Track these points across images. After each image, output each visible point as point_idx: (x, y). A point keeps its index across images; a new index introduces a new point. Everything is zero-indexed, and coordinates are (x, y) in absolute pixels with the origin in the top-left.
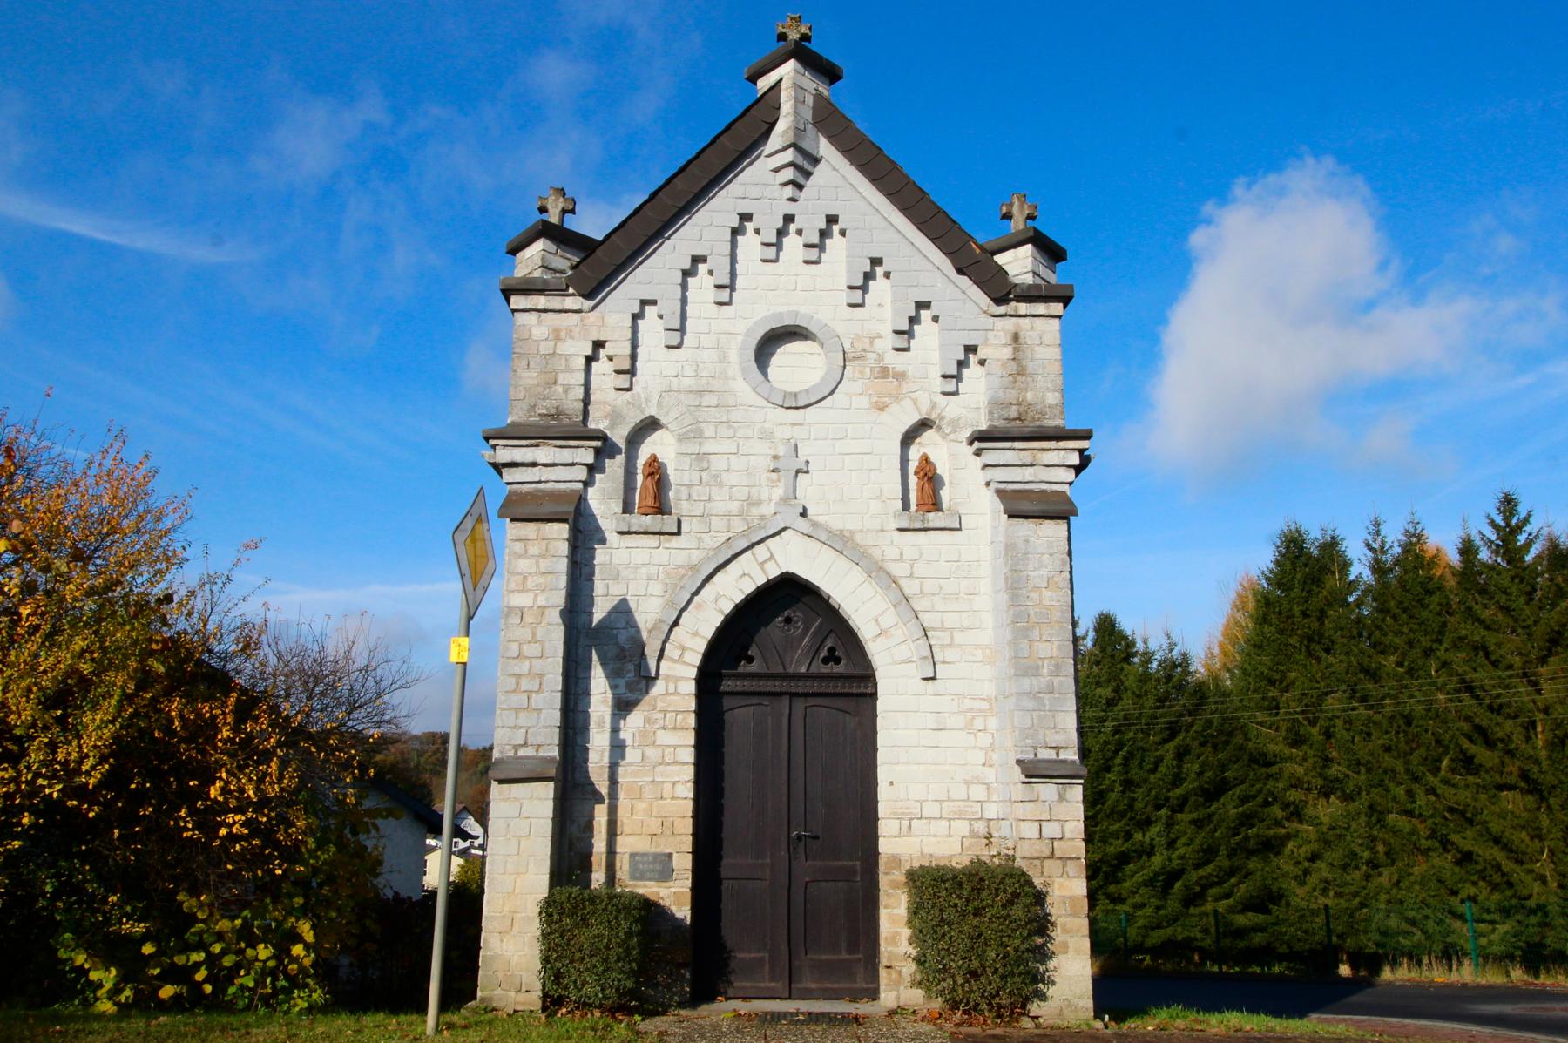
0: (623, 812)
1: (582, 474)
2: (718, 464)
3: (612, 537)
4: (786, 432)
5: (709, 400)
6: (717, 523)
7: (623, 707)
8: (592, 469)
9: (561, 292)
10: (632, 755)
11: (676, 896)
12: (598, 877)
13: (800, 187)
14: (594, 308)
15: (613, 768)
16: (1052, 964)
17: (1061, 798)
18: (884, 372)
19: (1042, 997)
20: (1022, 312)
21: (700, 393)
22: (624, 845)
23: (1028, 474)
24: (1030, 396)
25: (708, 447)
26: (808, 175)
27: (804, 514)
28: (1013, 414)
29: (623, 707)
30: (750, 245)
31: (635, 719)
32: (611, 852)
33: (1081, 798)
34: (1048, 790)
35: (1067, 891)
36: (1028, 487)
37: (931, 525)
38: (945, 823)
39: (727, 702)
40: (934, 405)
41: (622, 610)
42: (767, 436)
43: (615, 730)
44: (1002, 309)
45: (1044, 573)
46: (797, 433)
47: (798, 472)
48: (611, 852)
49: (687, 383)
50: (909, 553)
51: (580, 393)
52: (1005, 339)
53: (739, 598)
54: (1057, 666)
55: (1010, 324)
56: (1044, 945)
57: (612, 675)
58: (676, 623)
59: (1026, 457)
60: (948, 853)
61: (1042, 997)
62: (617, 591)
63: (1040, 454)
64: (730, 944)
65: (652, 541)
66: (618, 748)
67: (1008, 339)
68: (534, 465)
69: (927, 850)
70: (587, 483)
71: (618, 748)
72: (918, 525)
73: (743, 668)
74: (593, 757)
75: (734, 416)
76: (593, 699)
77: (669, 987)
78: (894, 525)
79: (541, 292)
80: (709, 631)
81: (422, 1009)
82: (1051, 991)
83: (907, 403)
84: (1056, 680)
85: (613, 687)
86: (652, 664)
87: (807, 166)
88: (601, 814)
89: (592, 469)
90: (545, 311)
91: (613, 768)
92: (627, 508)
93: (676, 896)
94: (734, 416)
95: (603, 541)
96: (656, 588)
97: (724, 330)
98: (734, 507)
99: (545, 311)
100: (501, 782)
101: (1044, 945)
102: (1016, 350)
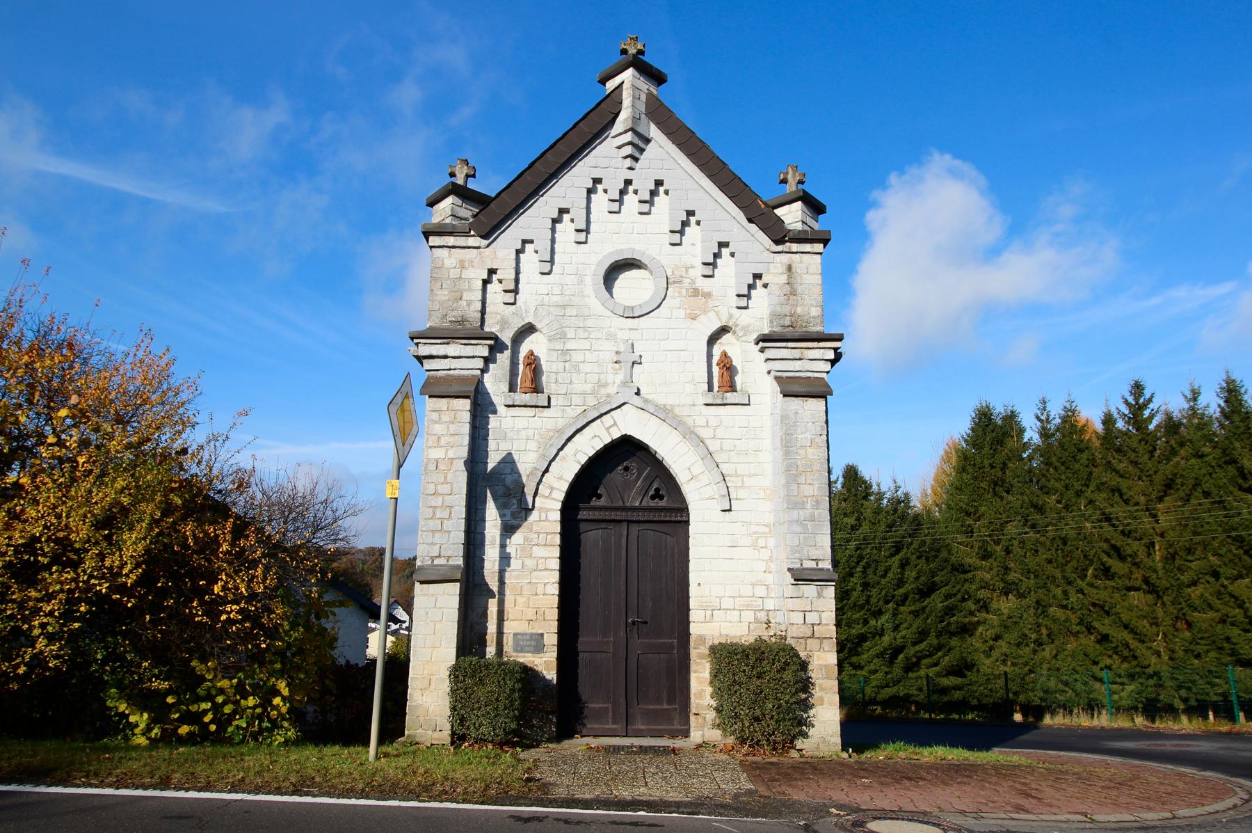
1: (480, 364)
2: (577, 357)
3: (501, 409)
5: (570, 311)
6: (576, 400)
7: (508, 529)
8: (488, 360)
10: (515, 564)
11: (546, 664)
12: (491, 650)
13: (636, 160)
14: (489, 245)
16: (812, 713)
17: (820, 595)
18: (696, 292)
19: (805, 735)
21: (564, 306)
22: (509, 628)
23: (797, 365)
24: (799, 310)
26: (642, 151)
27: (638, 393)
29: (508, 529)
30: (599, 200)
31: (517, 539)
32: (500, 632)
34: (810, 590)
35: (823, 661)
39: (583, 526)
40: (731, 316)
41: (508, 461)
43: (503, 546)
44: (780, 248)
45: (809, 436)
46: (633, 336)
48: (500, 632)
51: (479, 306)
56: (807, 698)
57: (501, 507)
59: (797, 354)
60: (739, 634)
61: (805, 735)
66: (505, 559)
69: (723, 632)
70: (484, 370)
71: (505, 559)
73: (595, 502)
75: (589, 323)
77: (541, 728)
79: (451, 234)
81: (366, 743)
82: (811, 732)
83: (712, 314)
84: (816, 512)
87: (641, 145)
88: (493, 605)
89: (488, 360)
90: (454, 247)
92: (512, 388)
93: (546, 664)
94: (589, 323)
95: (495, 412)
96: (532, 445)
98: (588, 388)
99: (454, 247)
101: (807, 698)
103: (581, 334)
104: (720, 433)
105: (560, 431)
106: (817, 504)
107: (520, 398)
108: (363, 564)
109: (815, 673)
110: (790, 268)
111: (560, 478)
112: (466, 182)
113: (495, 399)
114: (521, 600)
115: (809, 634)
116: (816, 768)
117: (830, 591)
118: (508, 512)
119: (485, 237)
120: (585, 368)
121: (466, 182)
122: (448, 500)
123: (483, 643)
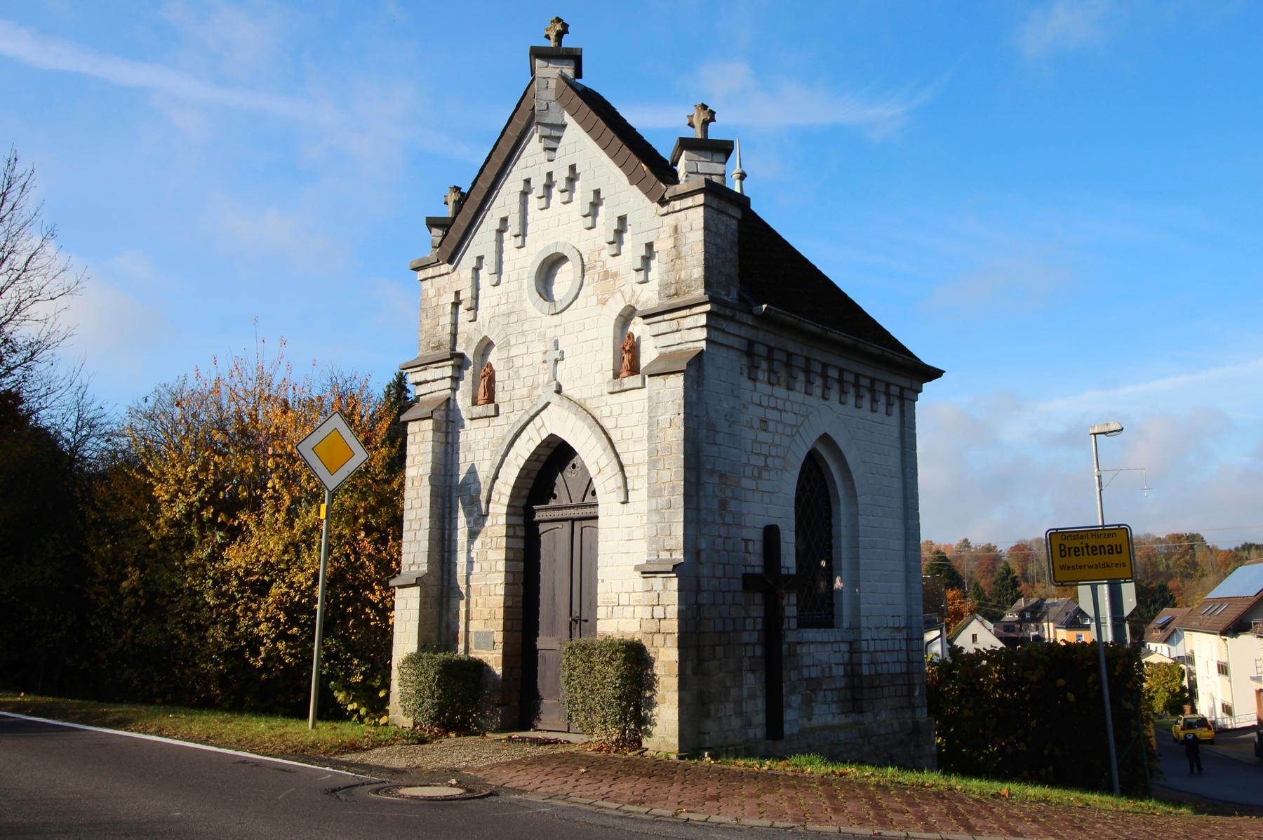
0: (472, 605)
1: (448, 383)
2: (518, 362)
3: (467, 422)
4: (551, 333)
5: (514, 318)
6: (518, 405)
7: (473, 535)
8: (456, 379)
9: (437, 263)
10: (476, 567)
11: (493, 658)
12: (461, 647)
13: (554, 150)
14: (454, 269)
15: (468, 575)
16: (655, 711)
17: (665, 587)
18: (606, 275)
19: (649, 734)
20: (677, 208)
21: (508, 315)
22: (474, 626)
23: (677, 338)
24: (683, 275)
25: (513, 352)
26: (559, 139)
27: (559, 391)
28: (673, 291)
29: (473, 535)
30: (534, 201)
31: (478, 543)
32: (467, 631)
33: (676, 587)
34: (657, 582)
35: (666, 658)
36: (679, 347)
37: (626, 387)
38: (631, 609)
39: (542, 528)
40: (633, 293)
41: (472, 472)
42: (542, 337)
43: (469, 551)
44: (665, 209)
45: (668, 416)
46: (557, 333)
47: (556, 361)
48: (467, 631)
49: (503, 308)
50: (616, 411)
51: (448, 329)
52: (669, 231)
53: (527, 456)
54: (673, 488)
55: (671, 219)
56: (651, 697)
57: (468, 514)
58: (496, 477)
59: (674, 324)
60: (633, 630)
61: (649, 734)
62: (470, 458)
63: (682, 321)
64: (541, 693)
65: (485, 422)
66: (470, 562)
67: (671, 232)
68: (427, 382)
69: (621, 629)
70: (454, 389)
71: (470, 562)
72: (618, 389)
73: (553, 503)
74: (459, 569)
75: (526, 327)
76: (459, 532)
77: (491, 719)
78: (605, 392)
79: (428, 266)
80: (512, 481)
81: (304, 716)
82: (655, 730)
83: (618, 295)
84: (672, 498)
85: (468, 523)
86: (483, 505)
87: (555, 133)
88: (462, 604)
89: (456, 379)
90: (433, 277)
91: (468, 575)
92: (474, 403)
93: (493, 658)
94: (526, 327)
95: (463, 427)
96: (487, 454)
97: (522, 262)
98: (525, 391)
99: (433, 277)
100: (400, 587)
101: (651, 697)
102: (676, 239)
103: (521, 340)
104: (622, 421)
105: (503, 439)
106: (672, 493)
107: (479, 410)
108: (1167, 559)
109: (659, 669)
110: (676, 229)
111: (506, 483)
112: (705, 131)
113: (464, 415)
114: (480, 601)
115: (655, 629)
116: (659, 770)
117: (674, 583)
118: (472, 519)
119: (450, 261)
120: (524, 372)
121: (705, 131)
122: (419, 511)
123: (456, 641)
